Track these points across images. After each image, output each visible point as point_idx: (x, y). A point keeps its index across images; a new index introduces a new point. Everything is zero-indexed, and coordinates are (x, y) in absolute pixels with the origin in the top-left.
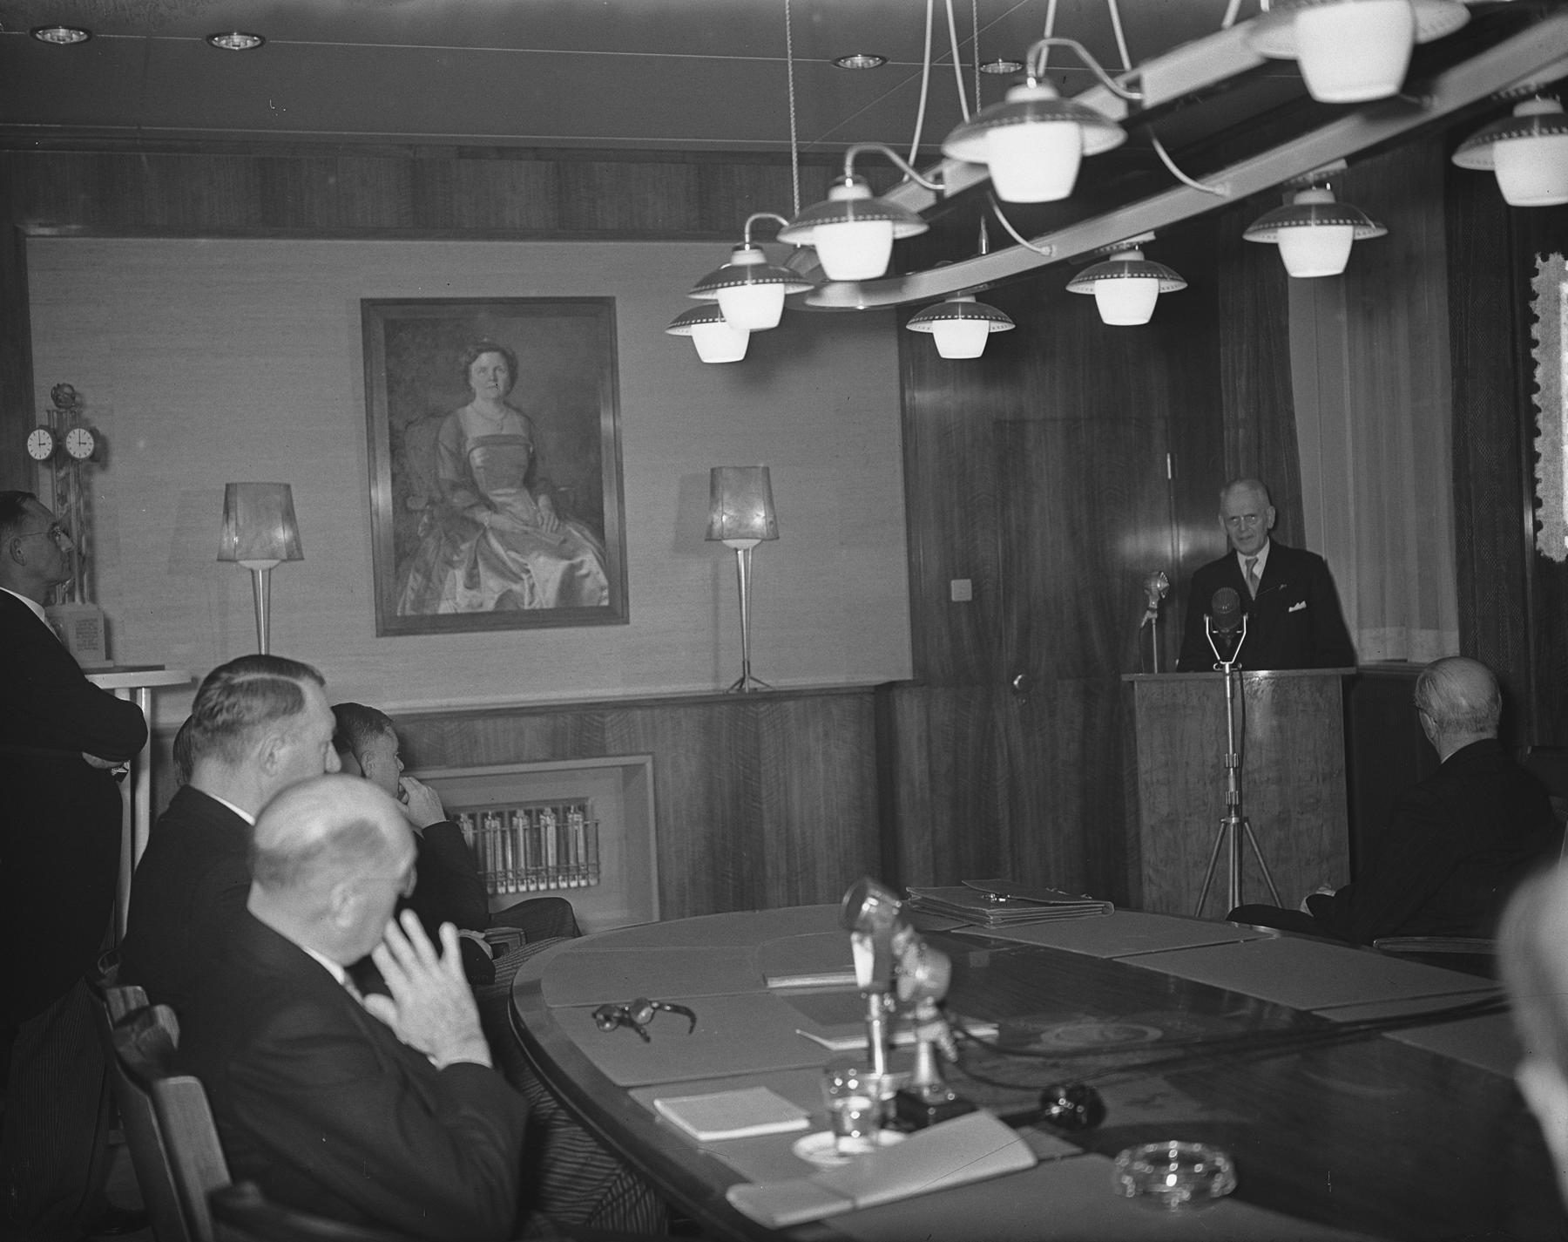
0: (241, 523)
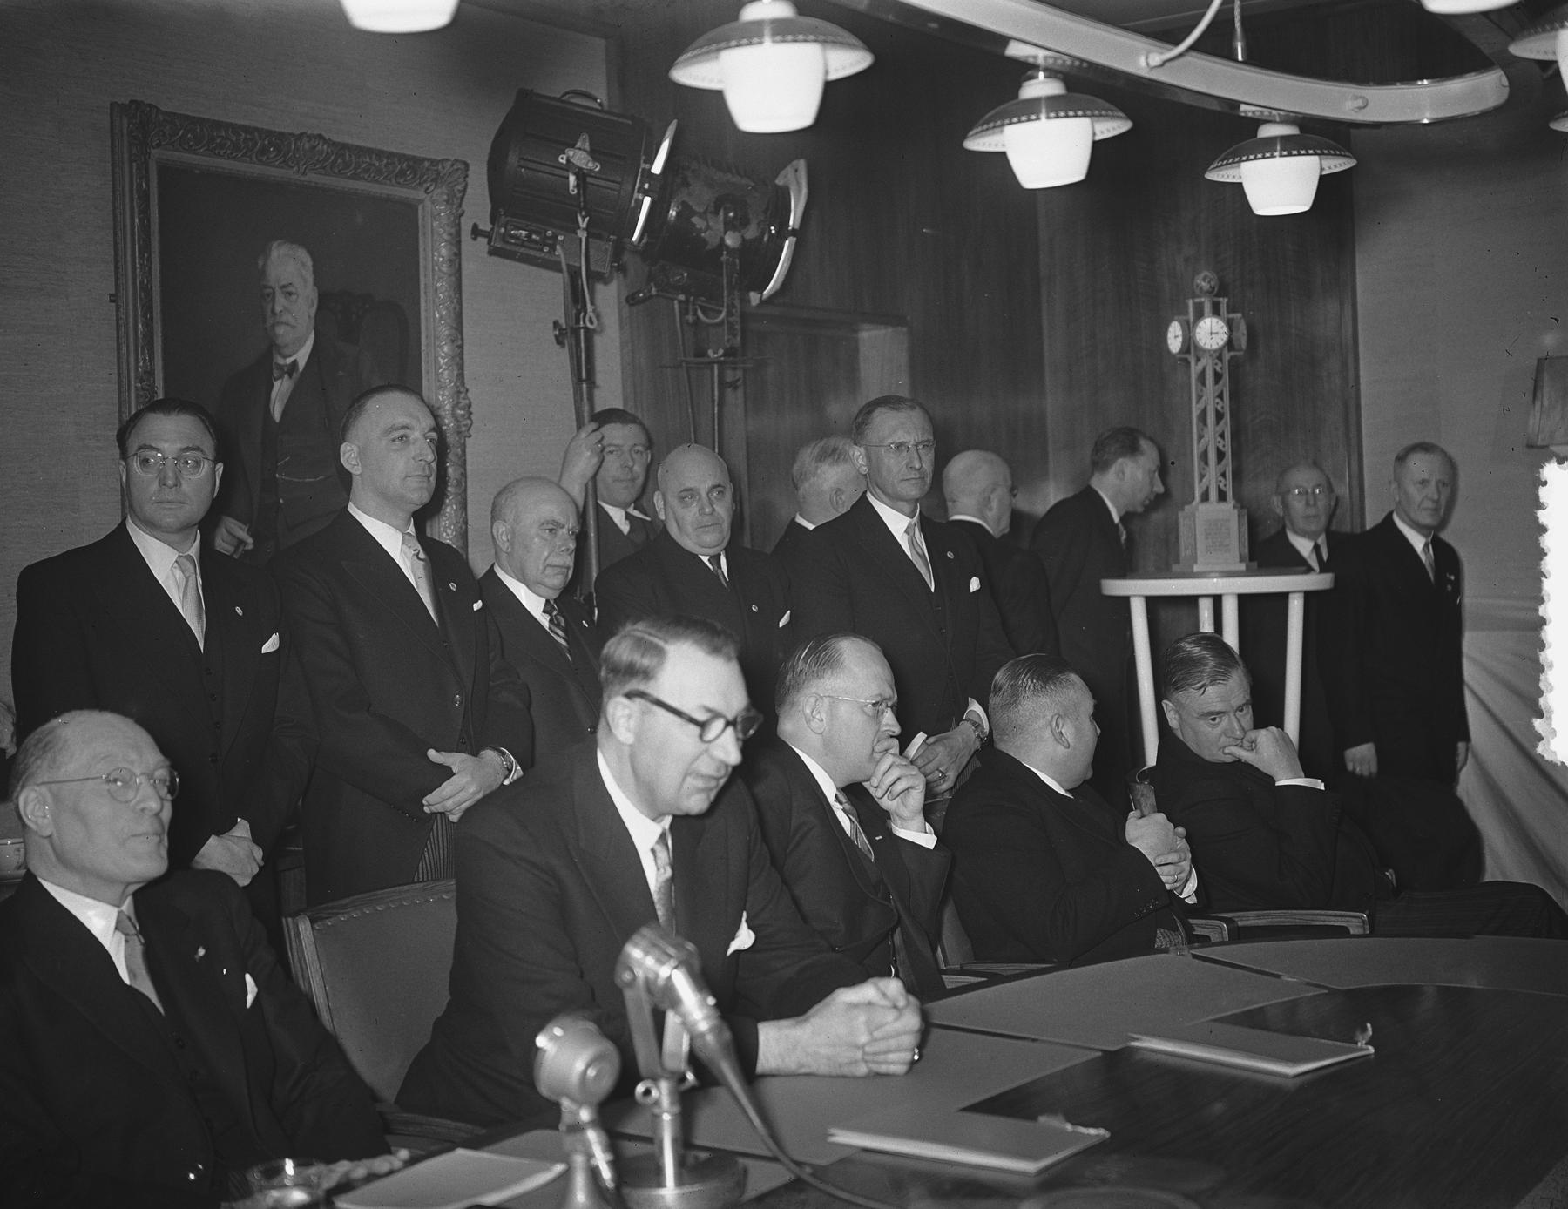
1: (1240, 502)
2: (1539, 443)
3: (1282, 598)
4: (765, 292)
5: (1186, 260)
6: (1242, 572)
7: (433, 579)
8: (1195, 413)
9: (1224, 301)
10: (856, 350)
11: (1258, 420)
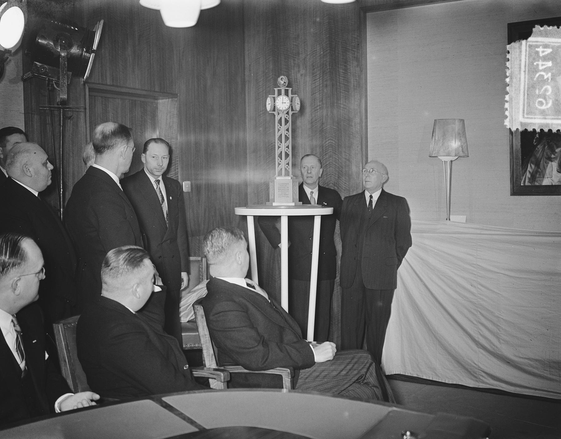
0: (437, 139)
1: (295, 176)
2: (433, 156)
3: (312, 218)
4: (85, 78)
5: (301, 75)
6: (293, 206)
7: (409, 212)
8: (277, 137)
9: (290, 89)
10: (157, 108)
11: (327, 143)
